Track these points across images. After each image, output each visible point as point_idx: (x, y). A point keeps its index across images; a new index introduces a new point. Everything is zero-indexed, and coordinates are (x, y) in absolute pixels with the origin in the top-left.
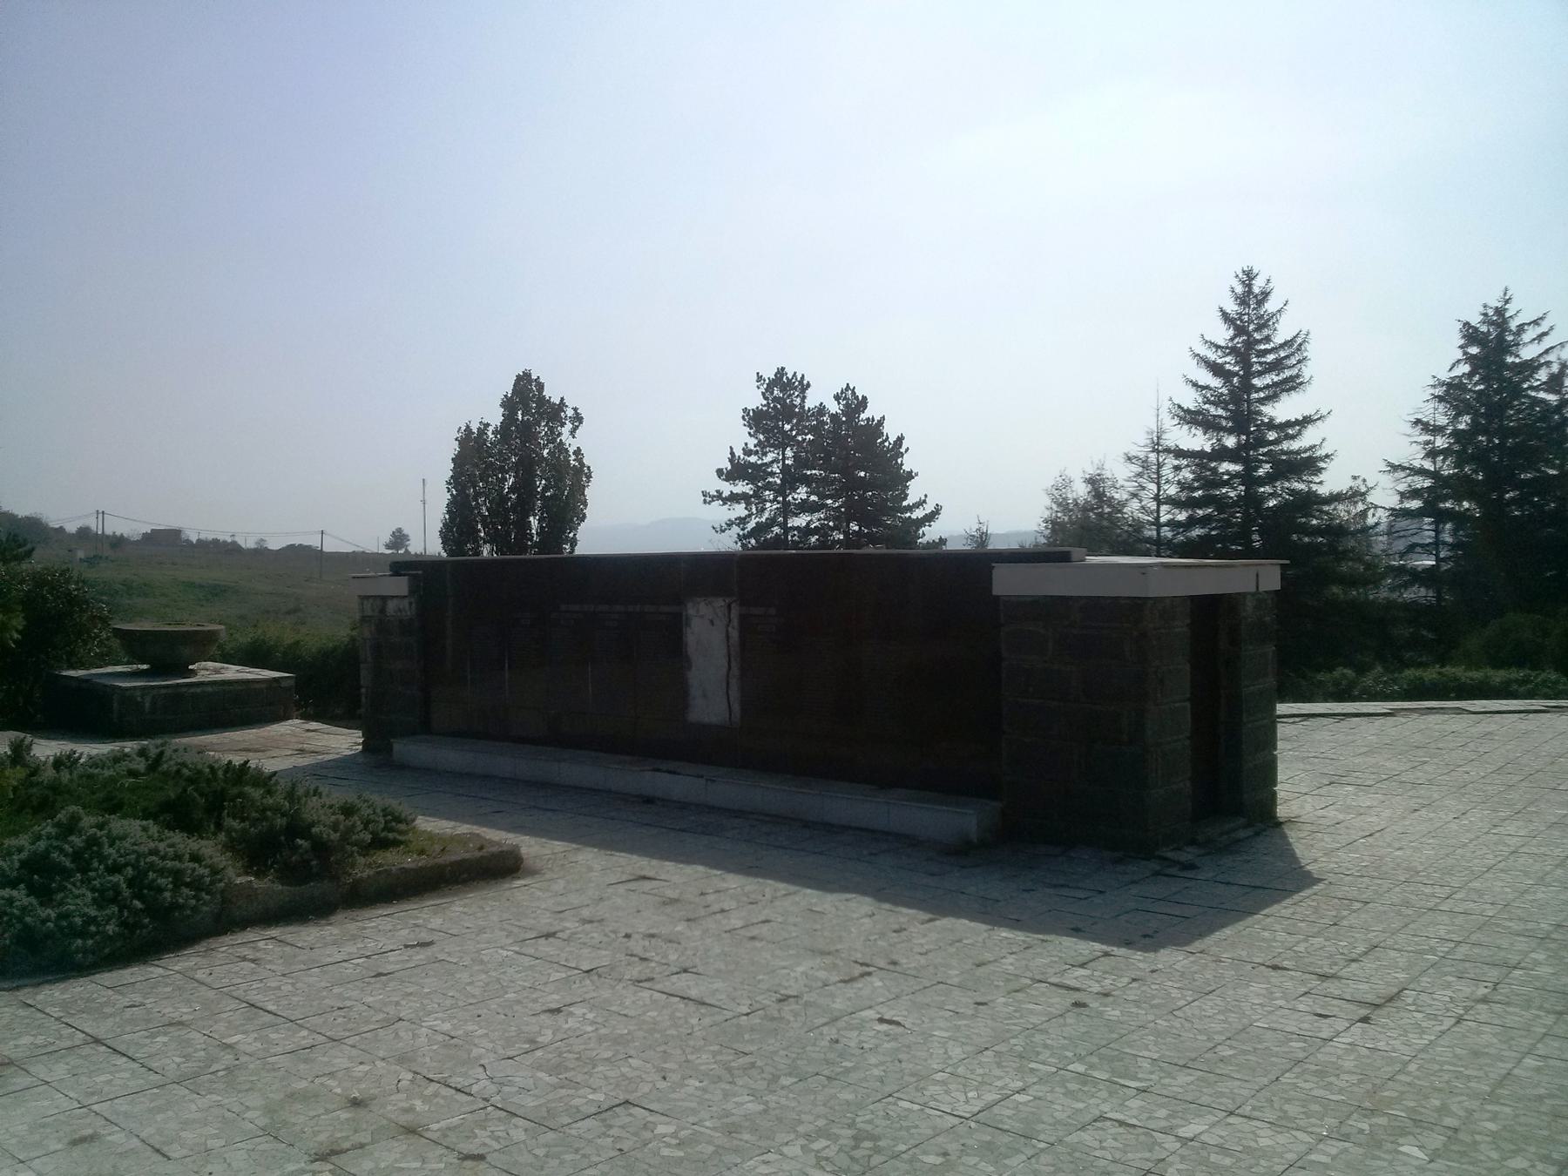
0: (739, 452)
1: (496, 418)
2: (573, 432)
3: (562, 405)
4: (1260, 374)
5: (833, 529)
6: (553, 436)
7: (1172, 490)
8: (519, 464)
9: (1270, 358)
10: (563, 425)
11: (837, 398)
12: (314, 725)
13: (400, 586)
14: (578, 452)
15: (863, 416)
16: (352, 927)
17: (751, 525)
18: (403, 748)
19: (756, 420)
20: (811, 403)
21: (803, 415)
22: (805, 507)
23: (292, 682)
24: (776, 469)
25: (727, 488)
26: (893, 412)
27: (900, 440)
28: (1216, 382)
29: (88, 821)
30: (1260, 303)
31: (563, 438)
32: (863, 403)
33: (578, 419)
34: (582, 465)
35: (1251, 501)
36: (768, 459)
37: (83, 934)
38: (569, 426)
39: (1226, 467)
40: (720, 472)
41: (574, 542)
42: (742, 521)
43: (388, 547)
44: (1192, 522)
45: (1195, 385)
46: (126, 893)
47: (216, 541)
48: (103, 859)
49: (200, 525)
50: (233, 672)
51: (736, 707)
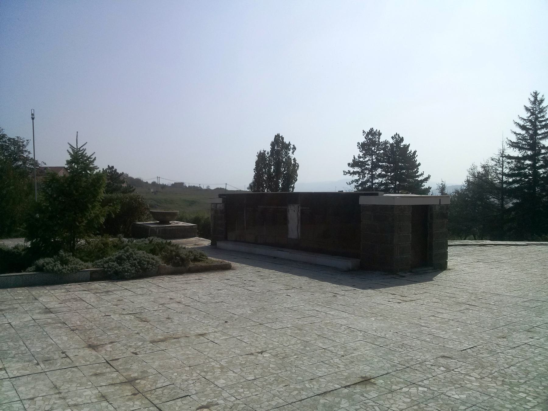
0: (356, 157)
1: (268, 149)
2: (293, 153)
3: (289, 144)
4: (540, 129)
5: (390, 183)
6: (287, 154)
7: (506, 171)
8: (277, 163)
9: (544, 123)
10: (290, 150)
11: (392, 138)
12: (202, 239)
13: (220, 201)
14: (294, 159)
15: (402, 144)
16: (186, 276)
17: (360, 182)
18: (220, 244)
19: (363, 146)
20: (382, 139)
21: (379, 144)
22: (380, 176)
23: (196, 227)
24: (369, 163)
25: (352, 170)
26: (413, 143)
27: (415, 152)
28: (523, 132)
29: (130, 250)
30: (540, 104)
31: (290, 155)
32: (402, 140)
33: (294, 148)
34: (296, 163)
35: (536, 174)
36: (367, 159)
37: (127, 272)
38: (292, 151)
39: (528, 162)
40: (349, 164)
41: (293, 188)
42: (357, 181)
43: (248, 189)
44: (514, 182)
45: (515, 133)
46: (137, 264)
47: (194, 187)
48: (133, 257)
49: (188, 182)
50: (181, 224)
51: (299, 234)
